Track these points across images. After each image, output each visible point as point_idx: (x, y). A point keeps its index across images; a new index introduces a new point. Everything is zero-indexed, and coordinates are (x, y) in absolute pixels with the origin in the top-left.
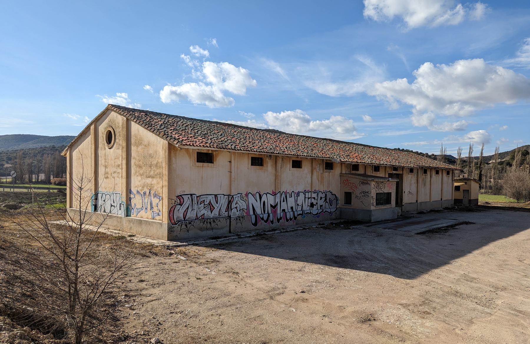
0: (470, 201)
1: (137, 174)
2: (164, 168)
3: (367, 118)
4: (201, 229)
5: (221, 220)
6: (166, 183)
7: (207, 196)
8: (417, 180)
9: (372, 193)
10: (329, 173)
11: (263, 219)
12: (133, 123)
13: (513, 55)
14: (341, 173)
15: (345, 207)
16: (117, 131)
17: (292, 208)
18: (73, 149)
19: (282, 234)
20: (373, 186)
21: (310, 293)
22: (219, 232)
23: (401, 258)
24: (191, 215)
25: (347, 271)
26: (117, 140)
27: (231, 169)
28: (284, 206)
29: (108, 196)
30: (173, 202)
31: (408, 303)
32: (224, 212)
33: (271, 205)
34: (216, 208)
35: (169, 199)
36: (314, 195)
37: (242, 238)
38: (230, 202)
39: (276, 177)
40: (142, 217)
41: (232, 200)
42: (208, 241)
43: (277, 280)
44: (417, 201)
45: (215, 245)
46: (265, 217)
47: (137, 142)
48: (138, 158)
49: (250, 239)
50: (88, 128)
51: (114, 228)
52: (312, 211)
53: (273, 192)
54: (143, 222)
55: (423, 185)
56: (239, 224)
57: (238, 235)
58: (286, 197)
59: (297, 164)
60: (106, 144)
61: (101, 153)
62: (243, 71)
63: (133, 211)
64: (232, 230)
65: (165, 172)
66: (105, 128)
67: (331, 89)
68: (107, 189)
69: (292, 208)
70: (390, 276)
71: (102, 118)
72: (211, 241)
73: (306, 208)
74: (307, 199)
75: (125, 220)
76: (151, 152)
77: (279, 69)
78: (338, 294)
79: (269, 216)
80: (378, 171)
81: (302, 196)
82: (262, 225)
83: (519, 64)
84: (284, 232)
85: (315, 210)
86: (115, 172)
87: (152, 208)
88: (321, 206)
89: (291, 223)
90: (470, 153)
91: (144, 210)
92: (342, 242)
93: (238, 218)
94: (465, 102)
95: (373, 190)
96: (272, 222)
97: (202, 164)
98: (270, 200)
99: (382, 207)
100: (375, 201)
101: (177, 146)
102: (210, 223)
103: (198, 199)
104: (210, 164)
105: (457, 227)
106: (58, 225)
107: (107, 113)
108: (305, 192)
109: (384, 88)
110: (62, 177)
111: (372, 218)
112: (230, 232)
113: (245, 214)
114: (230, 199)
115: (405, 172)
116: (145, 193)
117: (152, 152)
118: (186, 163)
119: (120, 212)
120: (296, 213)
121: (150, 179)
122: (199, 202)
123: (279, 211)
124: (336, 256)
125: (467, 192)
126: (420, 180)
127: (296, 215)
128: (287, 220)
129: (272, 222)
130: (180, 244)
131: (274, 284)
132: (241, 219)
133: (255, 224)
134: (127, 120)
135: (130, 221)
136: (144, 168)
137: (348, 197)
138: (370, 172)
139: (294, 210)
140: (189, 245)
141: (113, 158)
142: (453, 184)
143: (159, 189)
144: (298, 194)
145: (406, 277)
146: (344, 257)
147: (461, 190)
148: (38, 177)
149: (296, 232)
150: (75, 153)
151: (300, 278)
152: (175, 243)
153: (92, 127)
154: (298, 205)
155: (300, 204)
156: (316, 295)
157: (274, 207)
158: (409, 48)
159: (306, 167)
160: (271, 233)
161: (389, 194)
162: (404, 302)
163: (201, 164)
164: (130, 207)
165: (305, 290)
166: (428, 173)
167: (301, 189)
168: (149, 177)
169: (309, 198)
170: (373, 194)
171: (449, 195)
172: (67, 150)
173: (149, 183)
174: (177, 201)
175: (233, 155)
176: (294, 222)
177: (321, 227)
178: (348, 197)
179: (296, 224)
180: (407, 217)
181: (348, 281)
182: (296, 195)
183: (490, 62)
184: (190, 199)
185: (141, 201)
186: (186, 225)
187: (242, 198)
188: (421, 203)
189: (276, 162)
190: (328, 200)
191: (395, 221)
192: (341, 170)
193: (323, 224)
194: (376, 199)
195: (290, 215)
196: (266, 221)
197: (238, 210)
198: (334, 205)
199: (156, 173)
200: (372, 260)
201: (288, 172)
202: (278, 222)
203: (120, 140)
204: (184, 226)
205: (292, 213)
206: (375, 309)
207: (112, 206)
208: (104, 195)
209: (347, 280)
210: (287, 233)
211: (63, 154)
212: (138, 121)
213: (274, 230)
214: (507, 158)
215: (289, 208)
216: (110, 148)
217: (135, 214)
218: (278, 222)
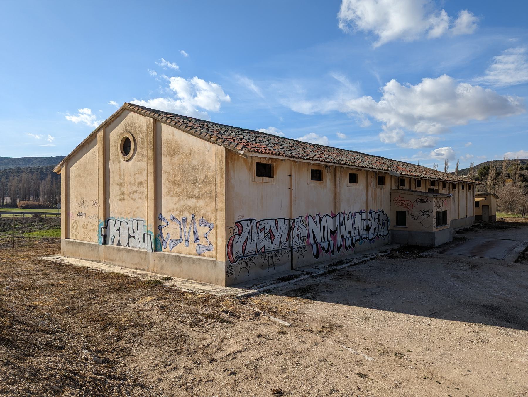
1: (172, 193)
2: (219, 185)
3: (341, 135)
4: (262, 267)
5: (283, 252)
6: (222, 205)
9: (434, 212)
11: (323, 248)
12: (164, 127)
13: (481, 72)
14: (391, 189)
15: (397, 229)
17: (350, 232)
18: (69, 164)
24: (251, 248)
26: (138, 150)
27: (291, 185)
28: (343, 231)
29: (124, 224)
32: (285, 242)
34: (276, 236)
35: (228, 227)
36: (369, 216)
39: (336, 195)
40: (179, 253)
41: (293, 226)
47: (171, 150)
48: (172, 172)
50: (94, 135)
51: (135, 267)
53: (332, 214)
56: (301, 257)
58: (344, 219)
60: (121, 155)
61: (113, 167)
62: (214, 85)
63: (164, 244)
64: (294, 268)
65: (221, 189)
66: (120, 135)
67: (305, 107)
68: (123, 215)
69: (350, 232)
71: (115, 122)
76: (194, 162)
77: (253, 87)
79: (329, 244)
83: (487, 82)
86: (135, 192)
87: (196, 239)
88: (375, 229)
90: (446, 168)
93: (302, 248)
94: (432, 119)
96: (333, 251)
97: (261, 178)
98: (329, 224)
101: (242, 152)
104: (270, 179)
106: (53, 262)
107: (123, 114)
108: (361, 212)
109: (356, 103)
110: (29, 200)
112: (292, 268)
113: (306, 244)
119: (144, 245)
121: (194, 201)
122: (259, 230)
125: (487, 208)
128: (347, 249)
133: (316, 256)
134: (156, 121)
135: (160, 258)
136: (183, 185)
137: (401, 218)
141: (132, 174)
142: (474, 200)
143: (209, 213)
147: (480, 205)
148: (3, 200)
150: (73, 169)
153: (100, 134)
157: (333, 232)
158: (406, 61)
163: (260, 178)
164: (160, 238)
166: (457, 188)
169: (364, 220)
172: (62, 165)
173: (192, 205)
174: (235, 229)
175: (293, 167)
176: (352, 250)
178: (401, 218)
179: (355, 253)
183: (460, 80)
184: (250, 225)
186: (246, 263)
190: (380, 222)
192: (391, 186)
195: (349, 242)
198: (386, 228)
202: (339, 252)
203: (143, 149)
204: (244, 264)
205: (350, 239)
207: (130, 236)
208: (118, 223)
211: (55, 170)
212: (173, 123)
215: (348, 233)
216: (127, 161)
217: (168, 248)
218: (339, 252)
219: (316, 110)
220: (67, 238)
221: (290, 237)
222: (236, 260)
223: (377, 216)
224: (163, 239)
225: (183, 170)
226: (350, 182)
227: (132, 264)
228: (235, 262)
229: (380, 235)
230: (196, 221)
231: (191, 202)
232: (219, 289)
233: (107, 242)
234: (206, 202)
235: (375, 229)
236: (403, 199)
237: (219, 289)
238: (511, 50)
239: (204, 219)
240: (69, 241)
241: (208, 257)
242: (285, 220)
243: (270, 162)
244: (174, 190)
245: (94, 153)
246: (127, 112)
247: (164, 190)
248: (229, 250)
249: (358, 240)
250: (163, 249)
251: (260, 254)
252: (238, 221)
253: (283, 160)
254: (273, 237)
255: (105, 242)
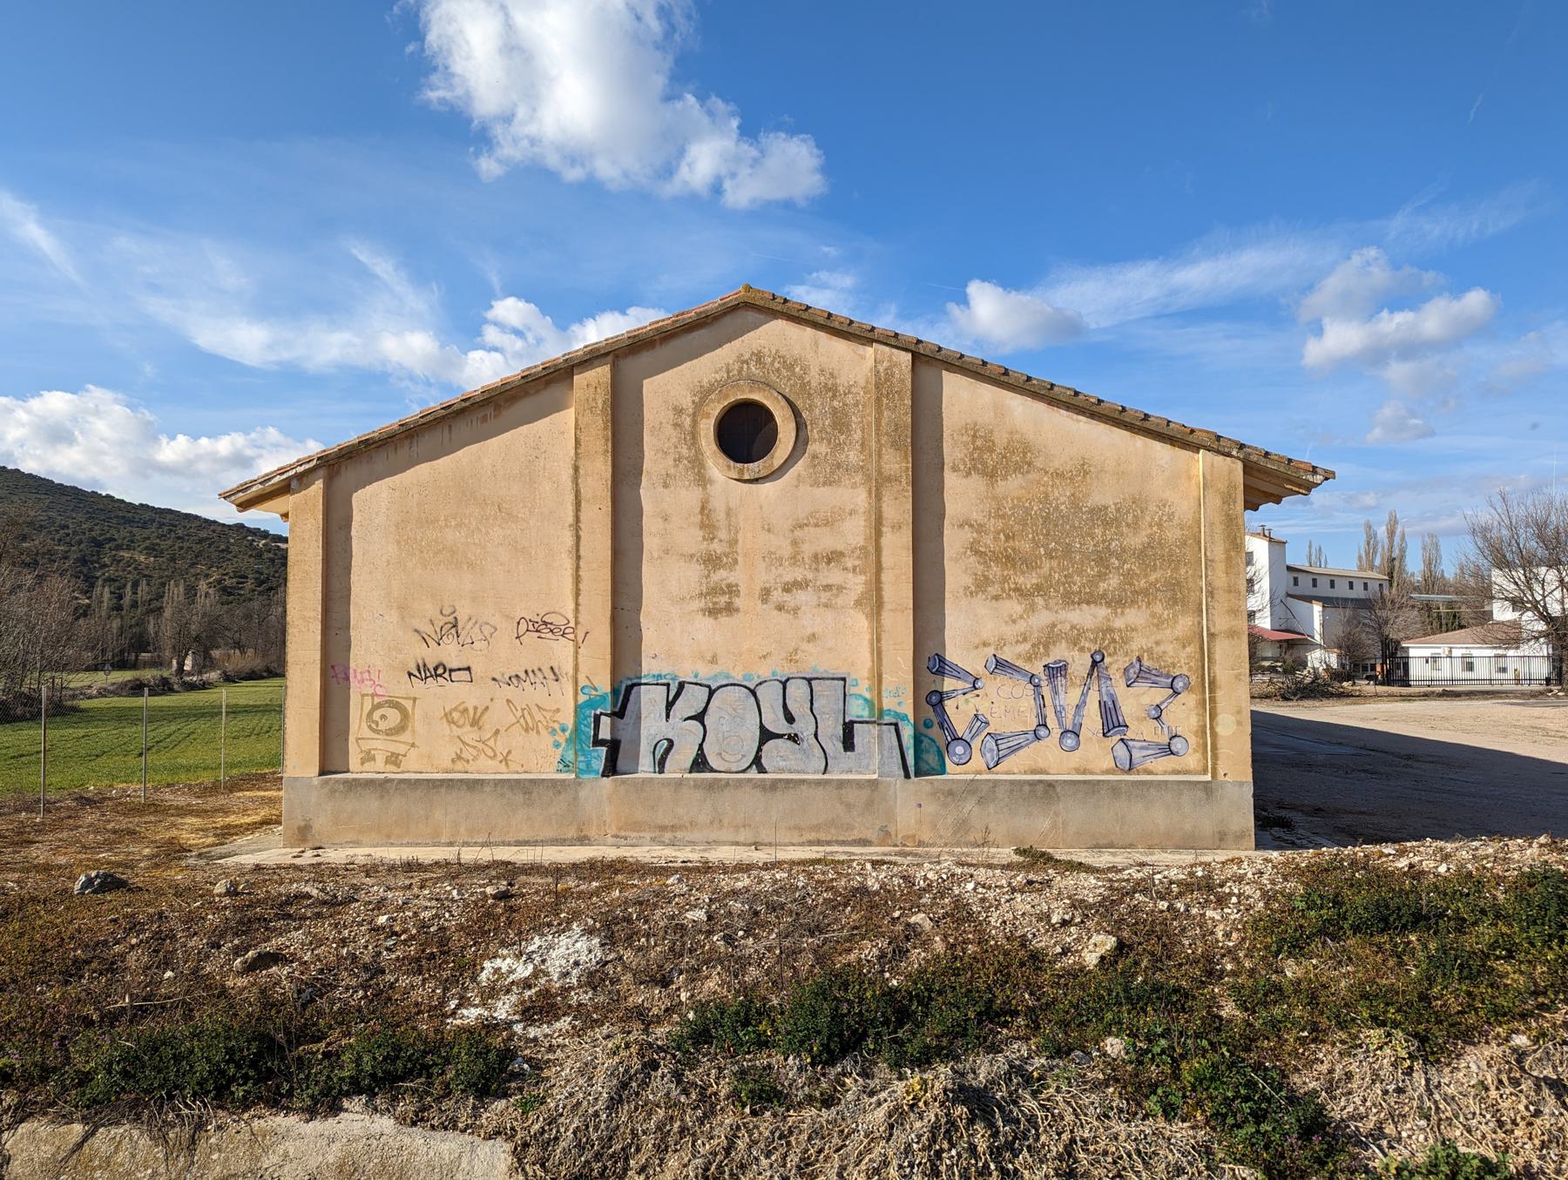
26: (816, 447)
51: (813, 836)
67: (248, 340)
77: (35, 233)
121: (1102, 612)
135: (952, 794)
207: (766, 735)
219: (286, 355)
220: (330, 760)
224: (952, 731)
225: (1046, 519)
227: (798, 828)
230: (1111, 672)
231: (1088, 617)
233: (621, 764)
234: (1153, 615)
238: (824, 276)
239: (1146, 663)
241: (1165, 773)
244: (1005, 579)
245: (561, 436)
246: (751, 316)
247: (956, 575)
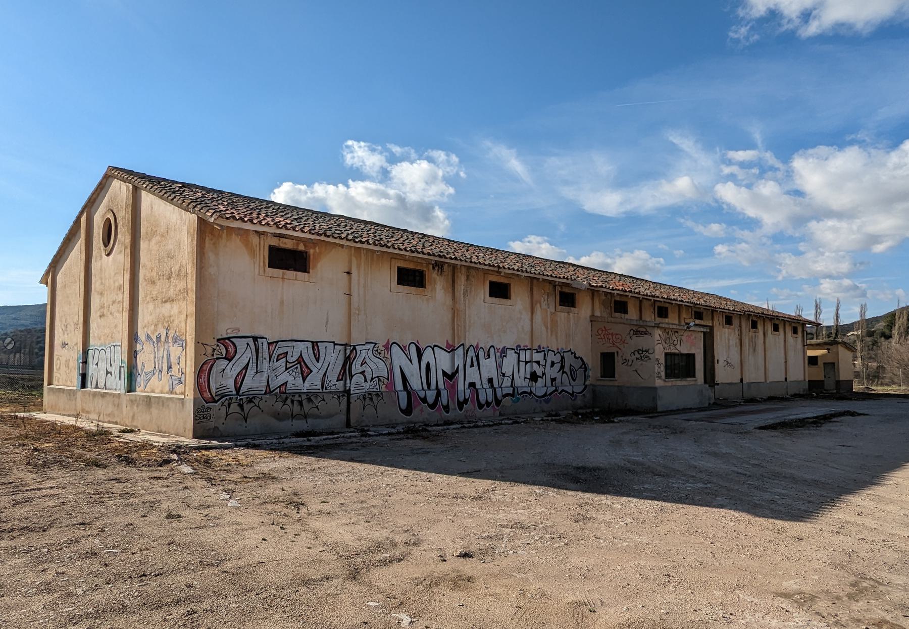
0: (838, 383)
4: (278, 416)
6: (192, 309)
7: (294, 343)
8: (741, 340)
9: (656, 352)
10: (568, 313)
11: (424, 400)
14: (593, 315)
16: (120, 217)
17: (490, 381)
19: (464, 430)
20: (657, 337)
21: (487, 558)
22: (322, 425)
23: (740, 471)
25: (606, 500)
26: (119, 236)
27: (350, 289)
28: (473, 375)
30: (209, 350)
31: (808, 589)
32: (334, 381)
33: (445, 373)
34: (315, 370)
36: (538, 357)
37: (370, 436)
38: (348, 361)
40: (153, 392)
41: (352, 356)
42: (287, 441)
43: (401, 522)
44: (742, 380)
45: (301, 446)
46: (431, 396)
49: (387, 438)
52: (533, 389)
54: (153, 400)
55: (751, 350)
56: (370, 410)
57: (362, 430)
58: (477, 357)
59: (500, 291)
61: (95, 266)
63: (139, 379)
64: (352, 421)
65: (191, 283)
67: (609, 202)
69: (490, 381)
70: (723, 512)
72: (295, 440)
73: (521, 382)
74: (522, 364)
75: (126, 398)
77: (516, 165)
78: (575, 560)
79: (439, 394)
80: (666, 316)
81: (511, 357)
82: (422, 413)
84: (470, 427)
85: (540, 388)
87: (170, 368)
88: (553, 380)
89: (489, 411)
91: (156, 375)
92: (596, 444)
93: (368, 396)
95: (659, 347)
97: (281, 271)
98: (443, 361)
99: (679, 383)
100: (663, 368)
102: (301, 403)
103: (272, 348)
105: (835, 419)
108: (518, 350)
111: (659, 403)
112: (348, 424)
113: (384, 389)
114: (348, 352)
115: (716, 322)
116: (159, 338)
117: (171, 247)
118: (242, 267)
120: (499, 391)
121: (168, 305)
122: (275, 356)
123: (461, 386)
124: (578, 468)
125: (831, 366)
126: (746, 341)
127: (499, 395)
128: (481, 406)
129: (446, 408)
130: (215, 443)
131: (386, 533)
132: (374, 398)
133: (408, 411)
137: (608, 361)
138: (649, 316)
139: (496, 385)
140: (236, 446)
141: (113, 274)
142: (804, 353)
144: (504, 352)
145: (767, 512)
146: (599, 469)
147: (820, 363)
149: (496, 427)
151: (471, 516)
152: (204, 442)
154: (504, 375)
155: (508, 372)
156: (505, 563)
157: (450, 377)
159: (519, 299)
160: (441, 428)
161: (691, 357)
162: (790, 585)
165: (473, 549)
166: (760, 327)
167: (509, 341)
168: (166, 301)
169: (526, 363)
170: (659, 353)
171: (798, 373)
174: (216, 348)
175: (354, 259)
176: (495, 410)
177: (552, 420)
179: (500, 415)
180: (729, 405)
181: (608, 524)
182: (498, 354)
184: (253, 347)
185: (152, 356)
186: (241, 406)
187: (377, 353)
188: (749, 384)
189: (453, 281)
190: (567, 369)
191: (702, 411)
193: (556, 415)
194: (666, 366)
196: (432, 406)
197: (369, 377)
199: (178, 290)
200: (668, 476)
201: (479, 304)
202: (461, 409)
203: (123, 236)
204: (234, 407)
205: (490, 391)
206: (702, 615)
207: (108, 373)
209: (605, 522)
210: (475, 430)
213: (448, 423)
214: (881, 325)
215: (485, 381)
218: (461, 409)
219: (629, 207)
221: (346, 371)
222: (217, 398)
223: (557, 359)
226: (491, 295)
228: (216, 402)
229: (563, 390)
232: (188, 441)
235: (553, 380)
236: (610, 332)
237: (188, 441)
240: (53, 389)
242: (335, 344)
243: (301, 247)
248: (202, 381)
249: (507, 395)
250: (138, 389)
251: (276, 395)
252: (225, 336)
253: (342, 246)
254: (305, 369)
255: (84, 385)
